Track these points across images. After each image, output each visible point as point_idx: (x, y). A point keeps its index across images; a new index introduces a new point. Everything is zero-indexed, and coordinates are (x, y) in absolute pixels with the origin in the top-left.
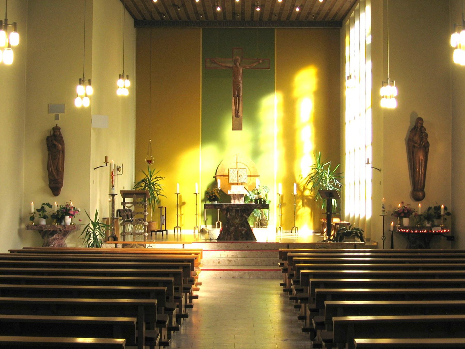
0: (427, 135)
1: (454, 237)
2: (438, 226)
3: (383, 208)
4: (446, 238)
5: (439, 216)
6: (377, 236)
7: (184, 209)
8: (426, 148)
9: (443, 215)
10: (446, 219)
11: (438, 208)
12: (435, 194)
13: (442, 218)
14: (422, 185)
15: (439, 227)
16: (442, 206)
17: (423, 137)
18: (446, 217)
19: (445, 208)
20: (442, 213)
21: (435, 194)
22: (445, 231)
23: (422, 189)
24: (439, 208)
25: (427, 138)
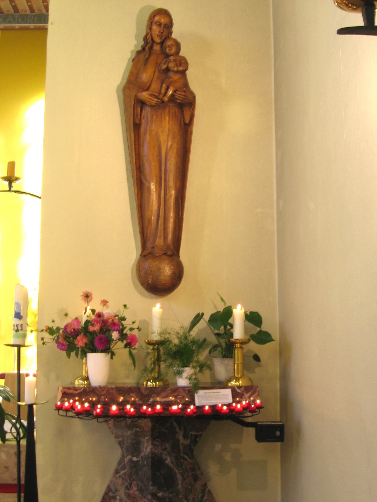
0: (183, 63)
1: (281, 428)
2: (222, 385)
3: (18, 316)
4: (252, 431)
5: (228, 349)
6: (156, 411)
7: (186, 376)
8: (183, 106)
9: (243, 343)
10: (256, 358)
11: (223, 318)
12: (219, 267)
13: (238, 353)
14: (170, 236)
15: (226, 387)
16: (239, 312)
17: (168, 70)
18: (253, 346)
19: (253, 318)
20: (238, 333)
21: (219, 267)
22: (244, 403)
23: (173, 251)
24: (228, 313)
25: (183, 73)
